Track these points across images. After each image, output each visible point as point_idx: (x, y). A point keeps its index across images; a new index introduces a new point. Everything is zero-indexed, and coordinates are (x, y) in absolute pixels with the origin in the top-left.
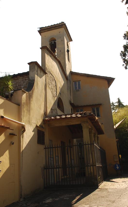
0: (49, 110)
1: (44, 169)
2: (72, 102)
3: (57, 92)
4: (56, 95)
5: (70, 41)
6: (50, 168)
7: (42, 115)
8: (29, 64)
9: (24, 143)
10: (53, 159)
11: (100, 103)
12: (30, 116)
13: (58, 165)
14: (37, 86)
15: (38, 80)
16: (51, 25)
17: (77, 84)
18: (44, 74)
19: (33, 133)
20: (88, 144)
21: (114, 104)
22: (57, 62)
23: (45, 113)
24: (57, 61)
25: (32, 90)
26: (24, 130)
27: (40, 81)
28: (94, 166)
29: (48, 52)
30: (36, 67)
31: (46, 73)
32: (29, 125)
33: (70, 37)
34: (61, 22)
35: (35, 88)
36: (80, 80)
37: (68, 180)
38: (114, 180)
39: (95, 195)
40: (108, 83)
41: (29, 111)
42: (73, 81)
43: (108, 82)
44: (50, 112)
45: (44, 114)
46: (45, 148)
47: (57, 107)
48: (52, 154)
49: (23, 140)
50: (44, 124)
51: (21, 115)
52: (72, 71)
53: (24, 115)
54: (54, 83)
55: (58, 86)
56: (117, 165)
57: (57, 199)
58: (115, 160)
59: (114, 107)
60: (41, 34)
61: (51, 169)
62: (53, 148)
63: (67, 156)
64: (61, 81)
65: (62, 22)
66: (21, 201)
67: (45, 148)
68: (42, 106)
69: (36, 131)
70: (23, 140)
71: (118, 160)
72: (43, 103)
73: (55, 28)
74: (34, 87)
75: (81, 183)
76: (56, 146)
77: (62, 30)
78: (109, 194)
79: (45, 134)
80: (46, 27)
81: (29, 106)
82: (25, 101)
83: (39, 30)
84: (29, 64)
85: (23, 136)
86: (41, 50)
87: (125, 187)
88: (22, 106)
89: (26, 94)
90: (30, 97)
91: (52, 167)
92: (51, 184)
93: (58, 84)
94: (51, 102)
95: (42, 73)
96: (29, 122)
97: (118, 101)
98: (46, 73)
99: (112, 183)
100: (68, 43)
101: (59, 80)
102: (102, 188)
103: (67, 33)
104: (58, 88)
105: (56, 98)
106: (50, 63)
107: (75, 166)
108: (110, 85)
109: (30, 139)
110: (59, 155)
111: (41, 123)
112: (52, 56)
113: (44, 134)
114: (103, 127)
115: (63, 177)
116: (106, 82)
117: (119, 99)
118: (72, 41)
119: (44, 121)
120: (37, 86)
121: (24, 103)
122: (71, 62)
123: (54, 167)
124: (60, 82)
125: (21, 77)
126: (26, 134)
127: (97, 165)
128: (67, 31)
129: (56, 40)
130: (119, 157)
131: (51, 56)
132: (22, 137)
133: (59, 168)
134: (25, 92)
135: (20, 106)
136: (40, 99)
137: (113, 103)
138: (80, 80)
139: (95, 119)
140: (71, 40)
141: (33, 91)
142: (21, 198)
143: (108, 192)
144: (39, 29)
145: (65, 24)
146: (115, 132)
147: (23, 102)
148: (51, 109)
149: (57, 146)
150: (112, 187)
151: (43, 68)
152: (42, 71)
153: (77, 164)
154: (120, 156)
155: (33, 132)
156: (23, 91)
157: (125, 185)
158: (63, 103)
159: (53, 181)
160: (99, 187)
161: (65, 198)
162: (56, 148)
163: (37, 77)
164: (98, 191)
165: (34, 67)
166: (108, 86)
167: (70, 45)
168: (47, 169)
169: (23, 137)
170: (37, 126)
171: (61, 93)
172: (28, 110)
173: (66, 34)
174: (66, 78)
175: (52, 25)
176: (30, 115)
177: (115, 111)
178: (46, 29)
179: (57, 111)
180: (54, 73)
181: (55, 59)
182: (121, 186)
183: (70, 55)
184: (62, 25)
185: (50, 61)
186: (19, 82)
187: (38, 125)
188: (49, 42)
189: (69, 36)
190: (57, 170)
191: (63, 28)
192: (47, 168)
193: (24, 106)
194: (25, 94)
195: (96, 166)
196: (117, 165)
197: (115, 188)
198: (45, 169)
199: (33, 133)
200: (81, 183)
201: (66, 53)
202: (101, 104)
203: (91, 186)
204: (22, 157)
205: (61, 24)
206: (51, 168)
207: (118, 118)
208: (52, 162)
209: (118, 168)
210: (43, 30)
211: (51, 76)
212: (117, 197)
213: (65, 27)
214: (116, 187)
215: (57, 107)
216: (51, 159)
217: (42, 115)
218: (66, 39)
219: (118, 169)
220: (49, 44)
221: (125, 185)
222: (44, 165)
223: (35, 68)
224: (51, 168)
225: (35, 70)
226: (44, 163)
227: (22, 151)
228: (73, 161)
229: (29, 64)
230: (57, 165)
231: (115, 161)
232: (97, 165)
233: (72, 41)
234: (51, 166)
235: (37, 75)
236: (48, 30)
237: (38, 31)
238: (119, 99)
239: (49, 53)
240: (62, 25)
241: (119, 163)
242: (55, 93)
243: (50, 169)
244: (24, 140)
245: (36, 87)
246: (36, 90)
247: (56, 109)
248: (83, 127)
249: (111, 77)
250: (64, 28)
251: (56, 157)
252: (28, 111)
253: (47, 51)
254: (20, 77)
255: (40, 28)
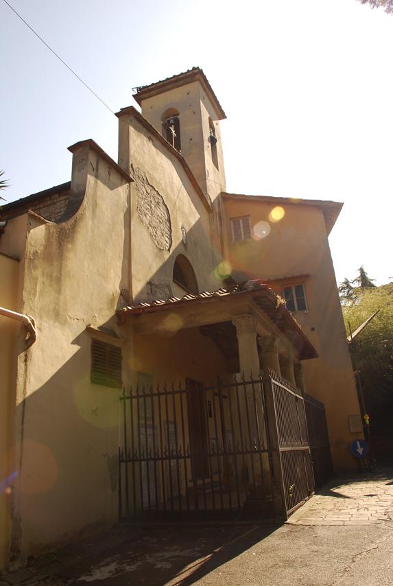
0: (137, 287)
1: (120, 461)
2: (185, 242)
3: (171, 239)
4: (170, 246)
5: (220, 119)
6: (159, 459)
7: (111, 298)
8: (71, 149)
9: (32, 379)
10: (152, 430)
11: (305, 274)
12: (62, 298)
13: (174, 448)
14: (94, 211)
15: (99, 193)
16: (165, 79)
17: (239, 225)
18: (124, 181)
19: (76, 348)
20: (253, 382)
21: (351, 285)
22: (176, 160)
23: (125, 294)
24: (173, 157)
25: (71, 221)
26: (33, 339)
27: (105, 200)
28: (262, 454)
29: (140, 126)
30: (92, 158)
31: (129, 180)
32: (57, 324)
33: (220, 107)
34: (191, 69)
35: (87, 215)
36: (249, 216)
37: (207, 491)
38: (343, 490)
39: (265, 551)
40: (325, 219)
41: (57, 281)
42: (231, 219)
43: (324, 214)
44: (142, 292)
45: (121, 294)
46: (121, 399)
47: (171, 279)
48: (149, 415)
49: (26, 370)
50: (119, 325)
51: (23, 288)
52: (227, 192)
53: (33, 292)
54: (161, 212)
55: (176, 222)
56: (358, 443)
57: (133, 568)
58: (352, 429)
59: (350, 292)
60: (142, 102)
61: (126, 461)
62: (152, 395)
63: (211, 421)
64: (187, 212)
65: (194, 68)
66: (11, 569)
67: (121, 399)
68: (112, 270)
69: (88, 342)
70: (26, 370)
71: (360, 428)
72: (119, 264)
73: (178, 84)
74: (80, 212)
75: (231, 505)
76: (169, 389)
77: (195, 86)
78: (315, 548)
79: (123, 354)
80: (153, 84)
81: (56, 264)
82: (40, 249)
83: (136, 92)
84: (71, 149)
85: (26, 355)
86: (116, 119)
87: (374, 519)
88: (26, 261)
89: (48, 229)
90: (62, 240)
91: (157, 454)
92: (146, 505)
93: (175, 219)
94: (148, 264)
95: (115, 178)
96: (57, 315)
97: (359, 275)
98: (129, 180)
99: (336, 499)
100: (214, 122)
101: (179, 208)
102: (300, 522)
103: (208, 95)
104: (176, 229)
105: (167, 256)
106: (147, 157)
107: (128, 458)
108: (333, 224)
109: (59, 367)
110: (155, 423)
111: (109, 321)
112: (153, 138)
113: (120, 354)
114: (315, 340)
115: (190, 484)
116: (319, 217)
117: (362, 271)
118: (224, 117)
119: (119, 316)
120: (94, 211)
121: (37, 252)
122: (224, 171)
123: (155, 456)
124: (183, 213)
125: (62, 198)
126: (43, 351)
127: (281, 449)
128: (208, 90)
129: (178, 114)
130: (364, 420)
131: (150, 139)
132: (23, 359)
133: (178, 457)
134: (42, 222)
135: (21, 262)
136: (105, 251)
137: (347, 282)
138: (249, 216)
139: (276, 302)
140: (222, 115)
141: (75, 221)
142: (13, 559)
143: (316, 540)
144: (135, 90)
145: (201, 72)
146: (350, 350)
147: (30, 249)
148: (150, 283)
149: (165, 389)
150: (332, 518)
151: (123, 167)
152: (113, 171)
153: (162, 452)
154: (367, 417)
155: (76, 346)
156: (31, 216)
157: (375, 508)
158: (196, 271)
159: (146, 499)
160: (288, 521)
161: (159, 566)
162: (163, 398)
163: (96, 183)
164: (283, 536)
165: (84, 158)
166: (326, 227)
167: (219, 128)
168: (129, 463)
169: (26, 361)
170: (89, 329)
171: (188, 245)
172: (51, 276)
173: (205, 95)
174: (205, 206)
175: (167, 79)
176: (59, 292)
177: (354, 303)
178: (153, 89)
179: (170, 291)
180: (163, 185)
181: (165, 149)
182: (362, 511)
183: (222, 151)
184: (195, 75)
185: (146, 151)
186: (57, 211)
187: (92, 326)
188: (162, 120)
189: (212, 99)
190: (173, 462)
191: (198, 82)
192: (149, 457)
193: (36, 262)
194: (42, 227)
195: (277, 450)
196: (358, 443)
197: (342, 523)
198: (123, 461)
199: (76, 348)
200: (231, 505)
201: (207, 144)
202: (307, 276)
203: (261, 513)
204: (23, 423)
205: (190, 73)
206: (124, 458)
207: (358, 315)
208: (150, 439)
209: (360, 450)
210: (145, 92)
211: (149, 192)
212: (342, 566)
213: (202, 80)
214: (346, 518)
215: (174, 281)
216: (148, 430)
217: (113, 299)
218: (205, 110)
219: (361, 453)
220: (163, 125)
221: (375, 508)
222: (119, 448)
223: (87, 159)
224: (124, 458)
225: (86, 165)
226: (121, 444)
227: (24, 401)
228: (229, 437)
229: (72, 152)
230: (130, 453)
231: (353, 433)
232: (281, 449)
233: (224, 117)
234: (147, 451)
235: (97, 177)
236: (159, 90)
237: (133, 95)
238: (362, 271)
239: (145, 130)
240: (195, 75)
241: (362, 437)
242: (165, 241)
243: (160, 462)
244: (31, 367)
245: (88, 213)
246: (90, 222)
247: (168, 286)
248: (237, 329)
249: (331, 202)
250: (200, 82)
251: (170, 425)
252: (51, 280)
253: (136, 122)
254: (59, 197)
255: (139, 89)
